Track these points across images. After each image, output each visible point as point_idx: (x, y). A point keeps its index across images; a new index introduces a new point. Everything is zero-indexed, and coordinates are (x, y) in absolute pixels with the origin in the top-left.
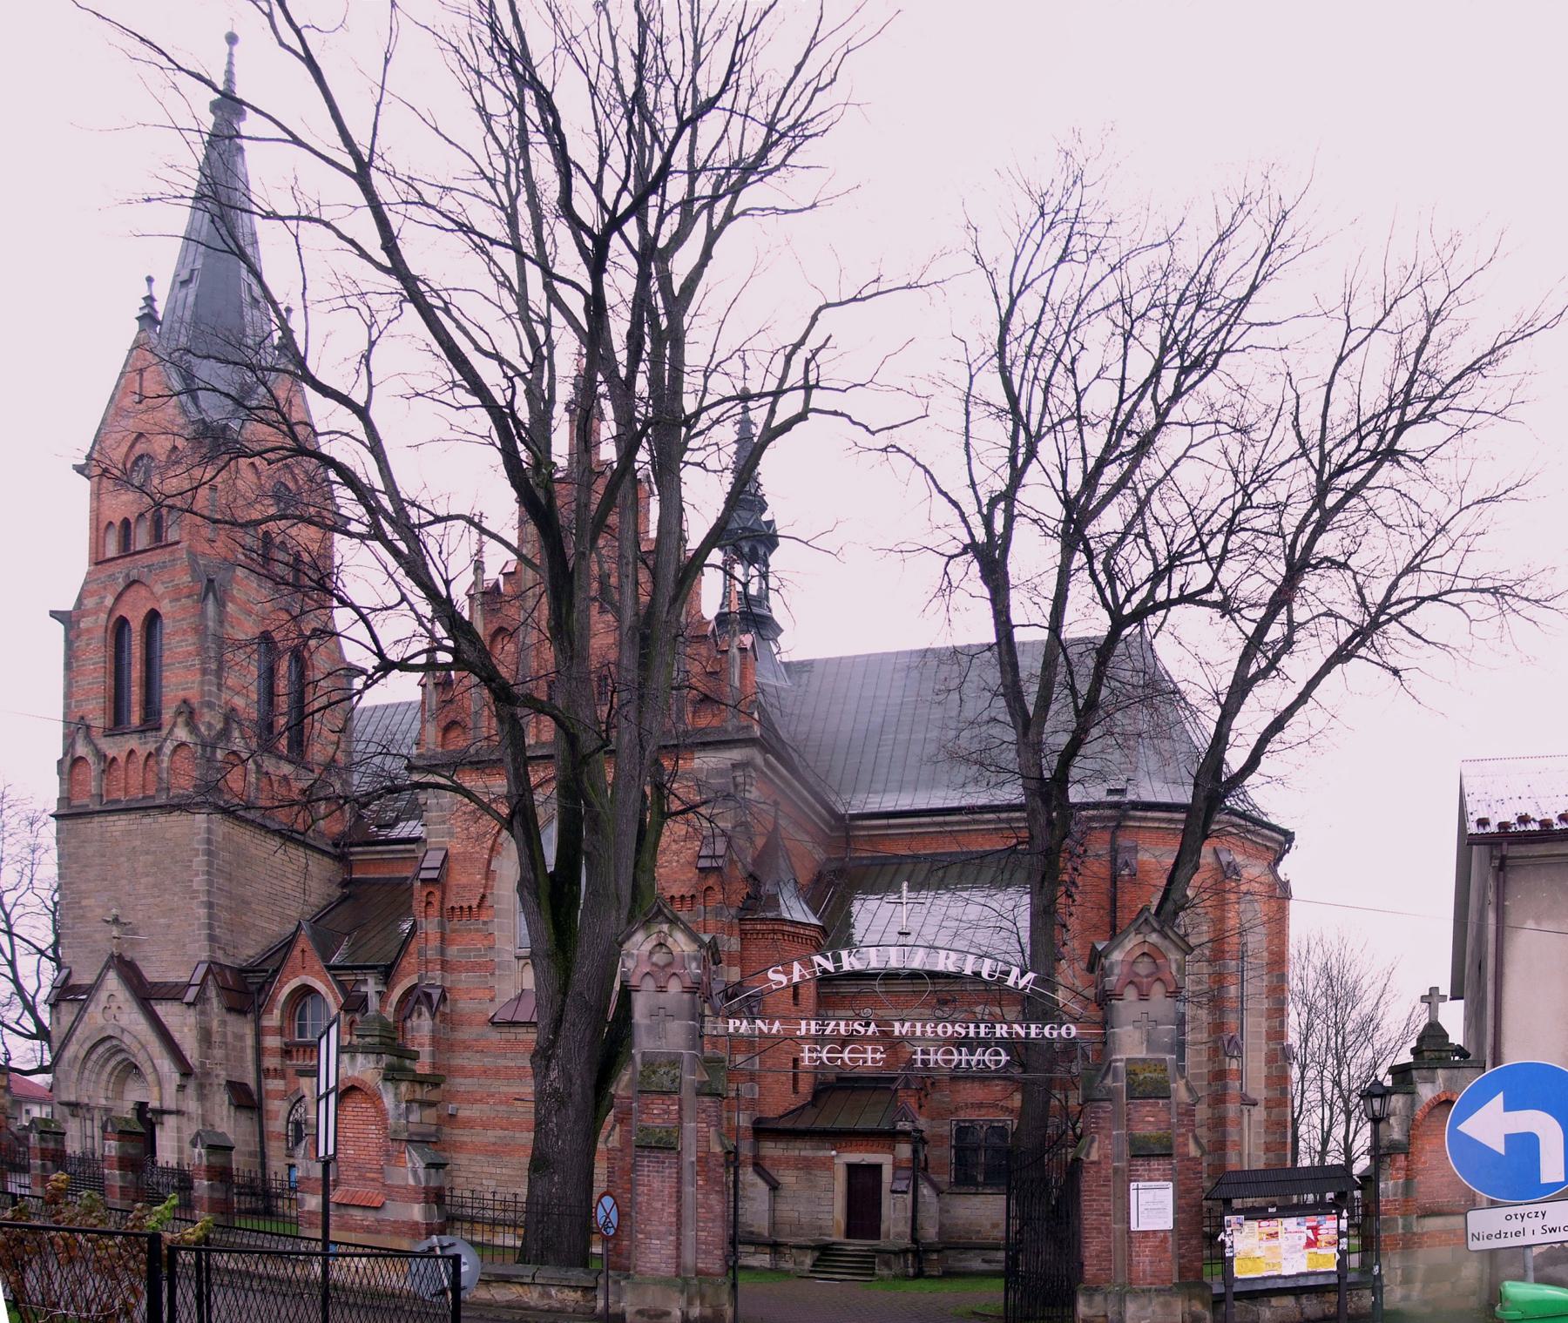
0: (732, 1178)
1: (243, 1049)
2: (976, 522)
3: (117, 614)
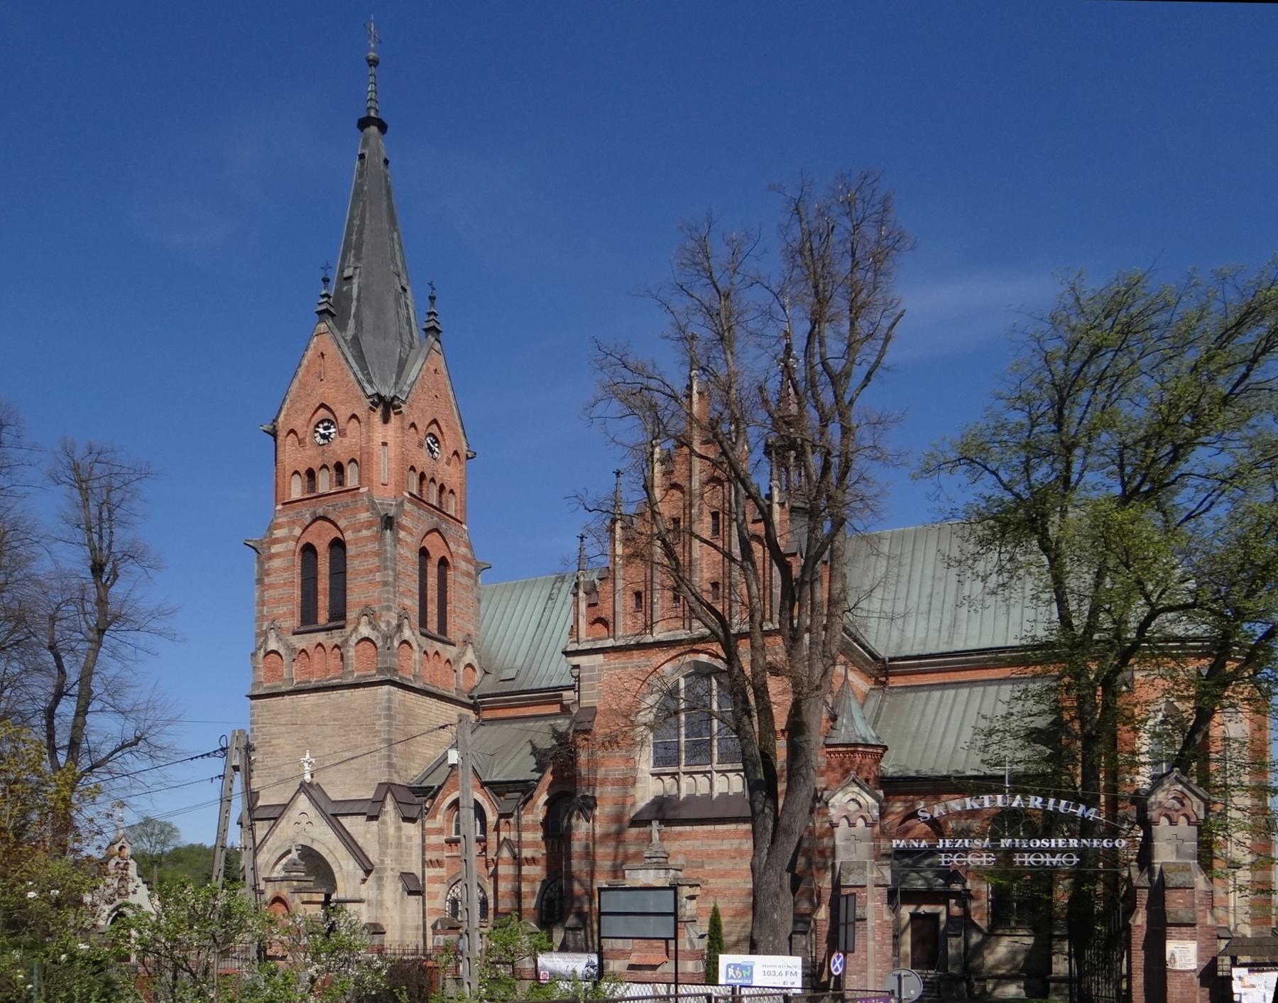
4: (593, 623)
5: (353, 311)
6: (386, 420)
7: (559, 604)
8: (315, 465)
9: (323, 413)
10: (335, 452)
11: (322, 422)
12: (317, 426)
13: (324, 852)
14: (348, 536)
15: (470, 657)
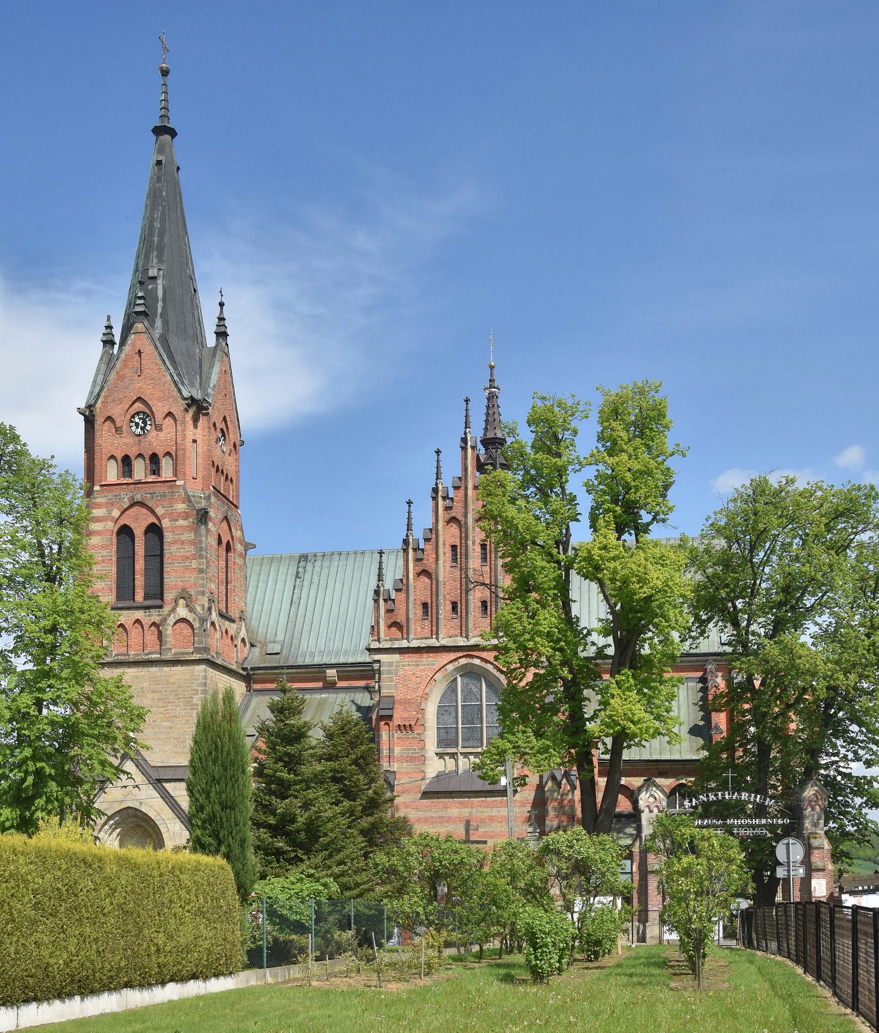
0: (285, 671)
2: (724, 503)
3: (121, 522)
4: (390, 627)
5: (159, 310)
6: (196, 420)
7: (306, 583)
8: (132, 452)
9: (139, 406)
10: (151, 444)
11: (138, 413)
12: (133, 417)
13: (152, 814)
14: (166, 523)
15: (243, 633)
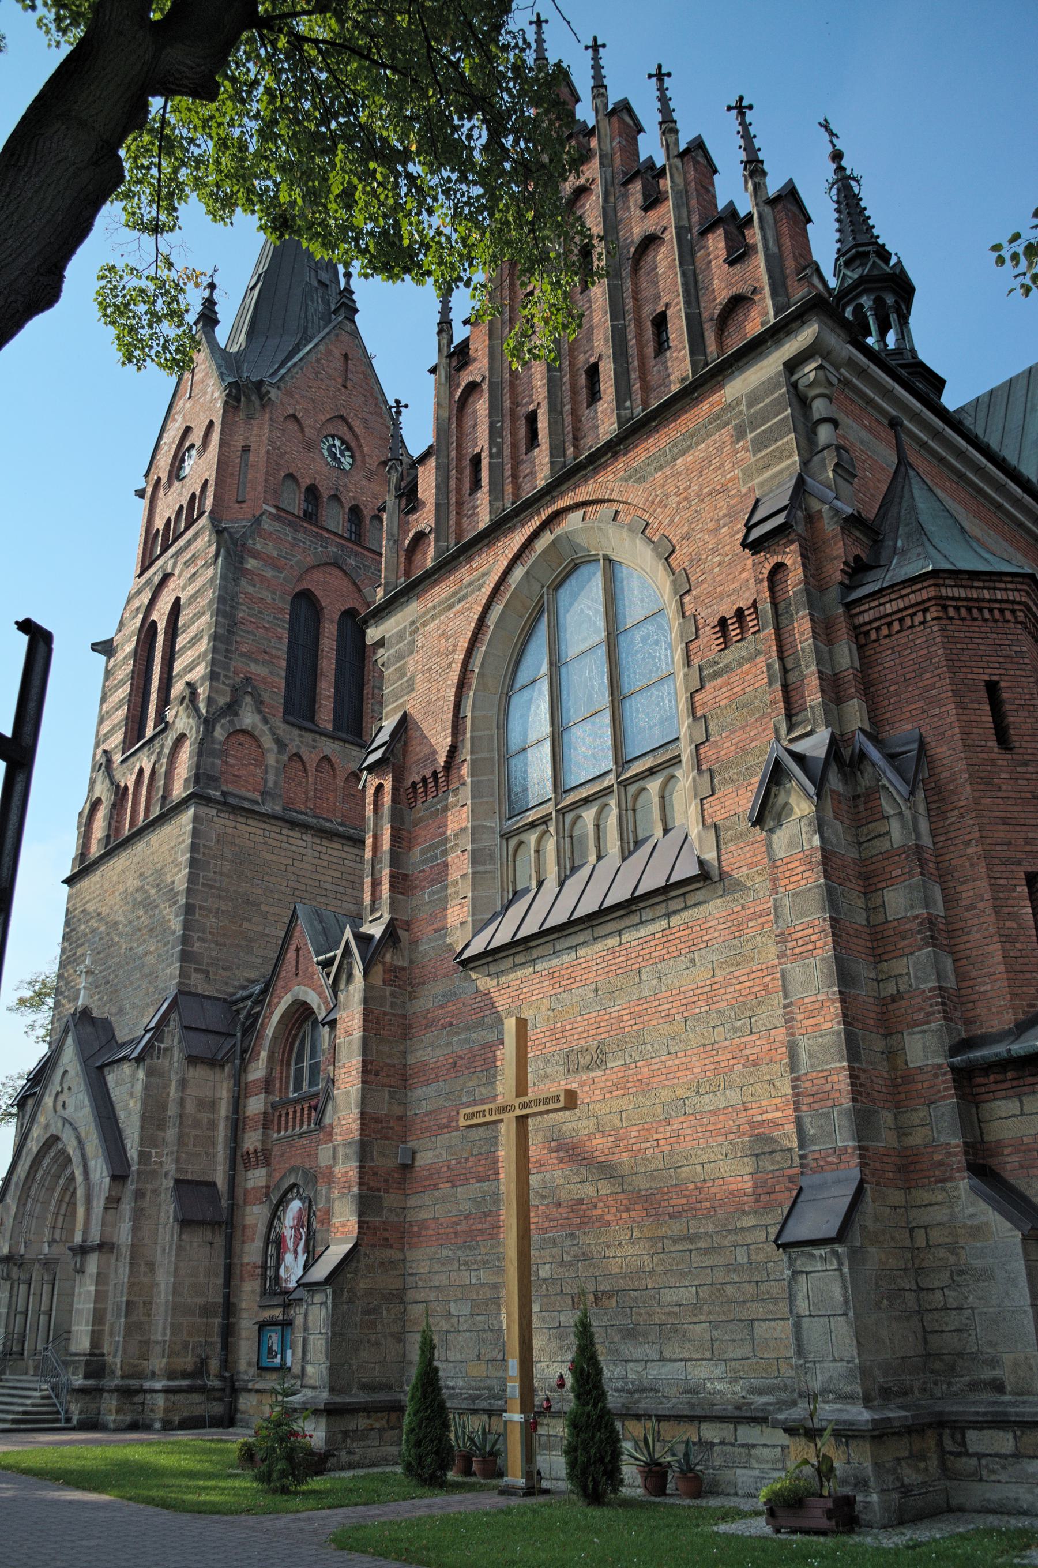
1: (212, 1125)
